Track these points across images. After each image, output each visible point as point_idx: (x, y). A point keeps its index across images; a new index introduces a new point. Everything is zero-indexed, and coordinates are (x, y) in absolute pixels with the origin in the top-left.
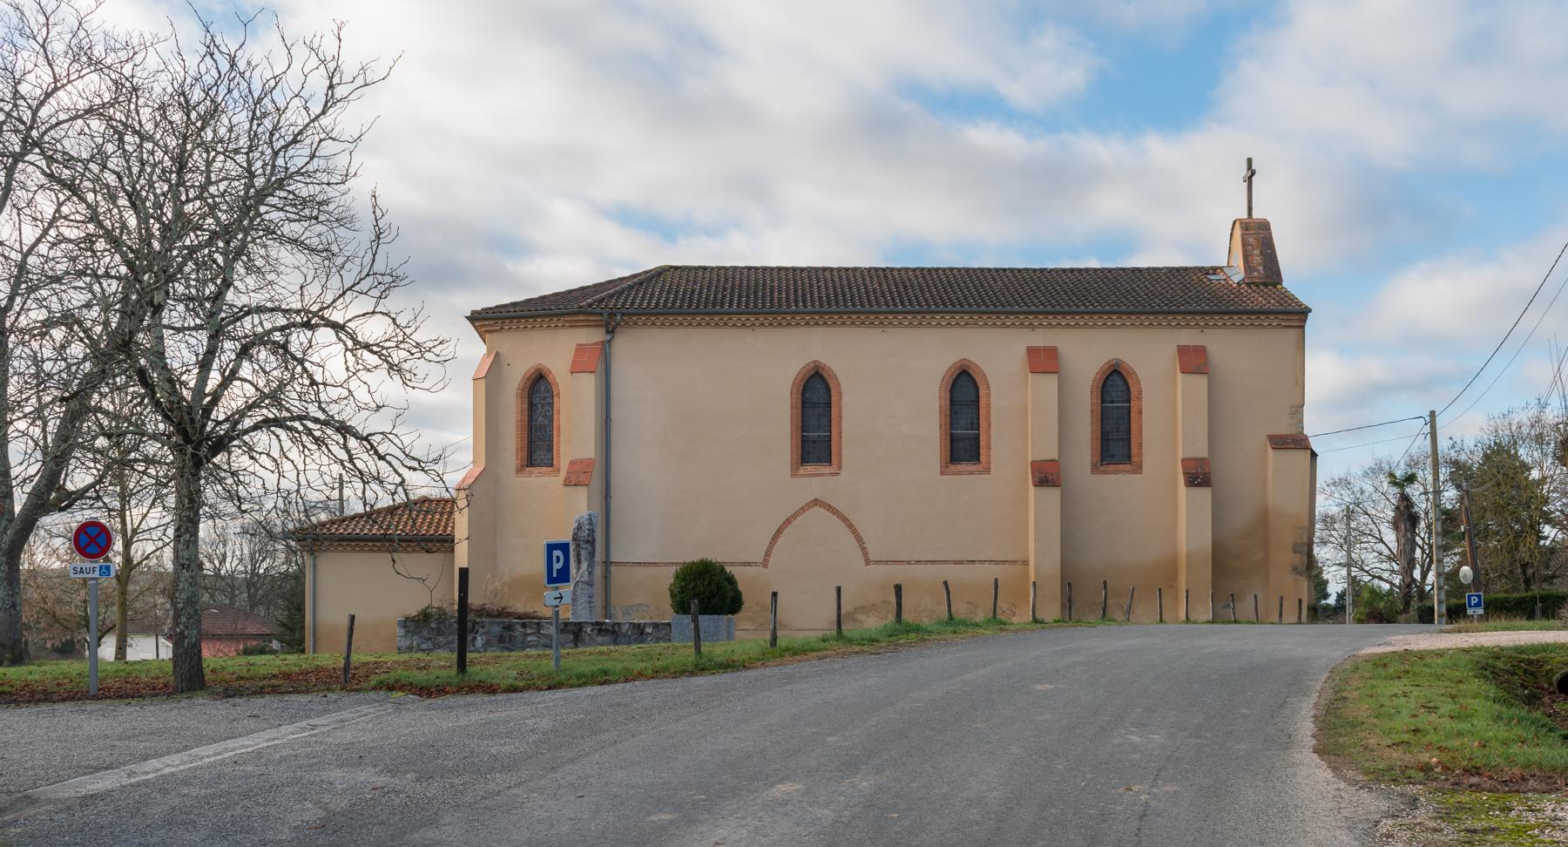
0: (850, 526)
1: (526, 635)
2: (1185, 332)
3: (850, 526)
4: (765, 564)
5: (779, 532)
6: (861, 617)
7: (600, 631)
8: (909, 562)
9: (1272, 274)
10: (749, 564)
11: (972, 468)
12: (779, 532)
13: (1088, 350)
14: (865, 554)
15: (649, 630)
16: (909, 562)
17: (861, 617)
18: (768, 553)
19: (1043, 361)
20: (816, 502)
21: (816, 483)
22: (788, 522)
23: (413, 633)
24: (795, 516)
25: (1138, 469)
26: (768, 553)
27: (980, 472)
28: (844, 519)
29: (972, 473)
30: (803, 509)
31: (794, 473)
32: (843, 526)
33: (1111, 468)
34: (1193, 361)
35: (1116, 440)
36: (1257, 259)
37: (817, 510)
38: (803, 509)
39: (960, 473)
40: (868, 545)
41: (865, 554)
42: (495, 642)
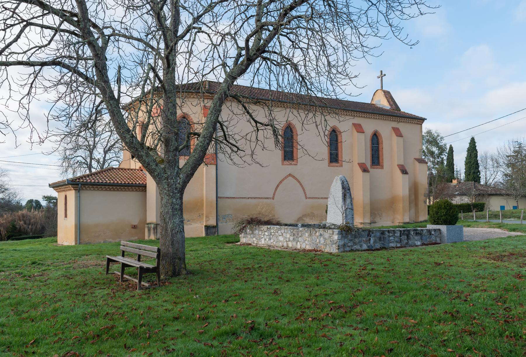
0: (301, 184)
1: (389, 236)
2: (394, 123)
3: (301, 184)
4: (273, 198)
5: (278, 186)
6: (305, 219)
7: (416, 233)
8: (319, 198)
9: (398, 108)
10: (267, 198)
11: (337, 165)
12: (278, 186)
13: (371, 125)
14: (306, 195)
15: (433, 233)
16: (319, 198)
17: (305, 219)
18: (274, 194)
19: (359, 128)
20: (290, 175)
21: (289, 168)
22: (281, 182)
23: (345, 237)
24: (283, 180)
25: (382, 167)
26: (274, 194)
27: (340, 166)
28: (299, 182)
29: (337, 166)
30: (286, 178)
31: (283, 164)
32: (298, 184)
33: (375, 166)
34: (398, 132)
35: (376, 158)
36: (392, 103)
37: (290, 178)
38: (286, 178)
39: (334, 166)
40: (307, 194)
41: (306, 195)
42: (378, 241)
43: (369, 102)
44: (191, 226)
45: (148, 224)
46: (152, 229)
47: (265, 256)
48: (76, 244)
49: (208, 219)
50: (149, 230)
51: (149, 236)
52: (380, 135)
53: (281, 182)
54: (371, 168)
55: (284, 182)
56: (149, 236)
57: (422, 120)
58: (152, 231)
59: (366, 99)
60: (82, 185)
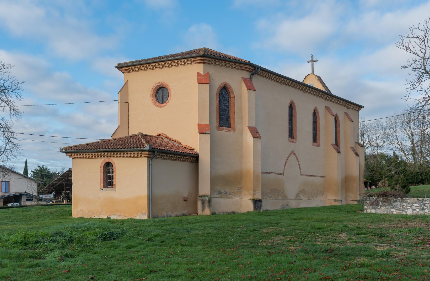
5: (286, 162)
18: (284, 171)
22: (287, 159)
26: (284, 171)
27: (317, 146)
31: (313, 145)
43: (301, 81)
44: (231, 200)
45: (201, 196)
46: (206, 202)
47: (228, 255)
48: (149, 217)
49: (255, 193)
50: (203, 203)
51: (203, 209)
52: (318, 113)
53: (287, 159)
54: (218, 128)
55: (289, 159)
56: (203, 209)
57: (360, 107)
58: (207, 204)
59: (301, 79)
60: (157, 152)
